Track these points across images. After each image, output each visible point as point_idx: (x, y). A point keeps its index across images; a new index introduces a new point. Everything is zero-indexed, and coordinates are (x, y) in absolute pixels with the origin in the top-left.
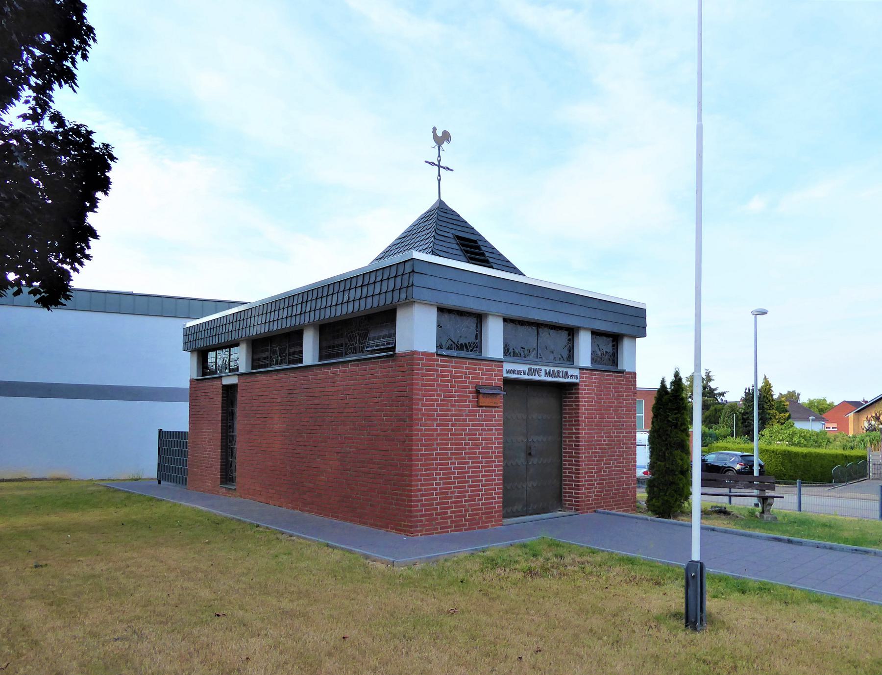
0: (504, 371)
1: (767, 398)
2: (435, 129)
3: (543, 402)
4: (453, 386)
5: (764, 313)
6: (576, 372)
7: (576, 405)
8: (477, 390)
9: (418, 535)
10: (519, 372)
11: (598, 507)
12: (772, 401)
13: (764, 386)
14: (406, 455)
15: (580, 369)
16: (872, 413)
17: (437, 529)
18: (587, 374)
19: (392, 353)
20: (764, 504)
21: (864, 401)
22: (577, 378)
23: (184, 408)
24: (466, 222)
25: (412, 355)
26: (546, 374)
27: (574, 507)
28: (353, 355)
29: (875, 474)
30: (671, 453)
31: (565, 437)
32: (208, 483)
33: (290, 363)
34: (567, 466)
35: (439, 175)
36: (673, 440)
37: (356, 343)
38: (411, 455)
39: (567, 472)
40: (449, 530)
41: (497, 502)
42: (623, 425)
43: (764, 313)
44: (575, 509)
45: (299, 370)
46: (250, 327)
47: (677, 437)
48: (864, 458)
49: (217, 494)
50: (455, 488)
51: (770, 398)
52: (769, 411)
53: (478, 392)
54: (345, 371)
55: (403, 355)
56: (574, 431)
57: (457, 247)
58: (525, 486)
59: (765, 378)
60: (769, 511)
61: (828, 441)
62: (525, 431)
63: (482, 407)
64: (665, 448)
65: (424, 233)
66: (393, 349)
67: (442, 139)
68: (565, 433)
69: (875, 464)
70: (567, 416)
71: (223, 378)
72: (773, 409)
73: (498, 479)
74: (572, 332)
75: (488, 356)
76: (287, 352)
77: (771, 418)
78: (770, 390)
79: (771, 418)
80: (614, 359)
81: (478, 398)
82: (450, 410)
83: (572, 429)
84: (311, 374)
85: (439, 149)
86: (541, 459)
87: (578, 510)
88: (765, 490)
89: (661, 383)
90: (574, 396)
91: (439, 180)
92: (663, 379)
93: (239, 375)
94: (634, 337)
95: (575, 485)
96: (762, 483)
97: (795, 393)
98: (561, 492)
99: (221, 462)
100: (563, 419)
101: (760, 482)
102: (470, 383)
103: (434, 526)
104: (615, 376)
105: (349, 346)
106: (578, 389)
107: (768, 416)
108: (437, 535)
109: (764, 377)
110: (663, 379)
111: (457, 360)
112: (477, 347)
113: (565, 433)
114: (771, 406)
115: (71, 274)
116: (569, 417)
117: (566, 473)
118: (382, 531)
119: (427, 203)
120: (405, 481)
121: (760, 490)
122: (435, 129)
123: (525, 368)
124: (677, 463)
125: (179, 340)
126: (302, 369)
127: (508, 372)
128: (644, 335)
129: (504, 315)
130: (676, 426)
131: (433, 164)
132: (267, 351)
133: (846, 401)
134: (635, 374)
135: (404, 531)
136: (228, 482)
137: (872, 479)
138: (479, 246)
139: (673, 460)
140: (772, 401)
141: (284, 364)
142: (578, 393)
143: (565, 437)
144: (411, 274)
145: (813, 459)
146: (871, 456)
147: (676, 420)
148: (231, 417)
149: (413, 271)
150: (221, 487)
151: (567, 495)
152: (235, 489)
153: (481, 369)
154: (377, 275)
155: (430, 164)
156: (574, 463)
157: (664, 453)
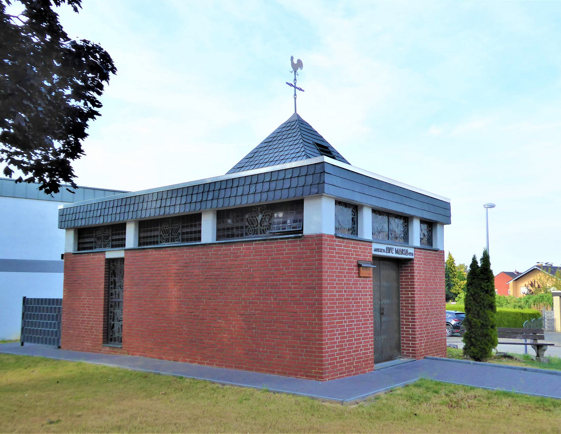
0: (373, 250)
1: (451, 269)
2: (292, 58)
3: (389, 273)
4: (345, 261)
5: (492, 206)
6: (411, 250)
7: (411, 276)
8: (358, 264)
9: (326, 380)
10: (381, 250)
11: (426, 354)
12: (455, 271)
13: (448, 260)
14: (316, 316)
15: (414, 248)
16: (527, 282)
17: (337, 375)
18: (418, 251)
19: (301, 235)
20: (539, 351)
21: (516, 272)
22: (413, 255)
23: (60, 277)
24: (317, 132)
25: (319, 238)
26: (397, 252)
27: (411, 355)
28: (255, 235)
29: (549, 327)
30: (484, 311)
31: (402, 300)
32: (87, 343)
33: (183, 240)
34: (404, 323)
35: (295, 95)
36: (486, 302)
37: (257, 226)
38: (321, 316)
39: (405, 328)
40: (344, 375)
41: (370, 354)
42: (438, 291)
43: (492, 206)
44: (412, 356)
45: (197, 247)
46: (109, 208)
47: (489, 300)
48: (536, 316)
49: (98, 352)
50: (336, 343)
51: (454, 269)
52: (453, 279)
53: (359, 266)
54: (250, 248)
55: (310, 237)
56: (410, 295)
57: (318, 152)
58: (380, 339)
59: (450, 254)
60: (543, 355)
61: (507, 302)
62: (379, 296)
63: (361, 277)
64: (480, 308)
65: (290, 140)
66: (301, 231)
67: (297, 66)
68: (402, 297)
69: (549, 320)
70: (404, 284)
71: (106, 253)
72: (456, 277)
73: (371, 334)
74: (407, 219)
75: (364, 238)
76: (180, 231)
77: (454, 285)
78: (453, 262)
79: (454, 285)
80: (430, 241)
81: (359, 270)
82: (343, 280)
83: (408, 294)
84: (211, 251)
85: (295, 74)
86: (389, 318)
87: (415, 357)
88: (537, 340)
89: (473, 259)
90: (409, 268)
91: (295, 98)
92: (474, 256)
93: (125, 250)
94: (443, 224)
95: (412, 338)
96: (534, 334)
97: (464, 266)
98: (399, 344)
99: (104, 325)
100: (400, 287)
101: (533, 333)
102: (354, 258)
103: (336, 372)
104: (434, 254)
105: (249, 228)
106: (413, 263)
107: (452, 283)
108: (338, 379)
109: (448, 253)
110: (474, 256)
111: (346, 241)
112: (355, 231)
113: (402, 297)
114: (454, 275)
115: (71, 165)
116: (405, 285)
117: (403, 328)
118: (292, 378)
119: (285, 116)
120: (315, 336)
121: (534, 340)
122: (292, 58)
123: (384, 247)
124: (490, 320)
125: (55, 219)
126: (201, 246)
127: (375, 250)
128: (449, 223)
129: (373, 207)
130: (487, 292)
131: (291, 85)
132: (157, 230)
133: (503, 272)
134: (444, 251)
135: (315, 377)
136: (109, 342)
137: (547, 331)
138: (330, 151)
139: (486, 318)
140: (455, 271)
141: (176, 242)
142: (413, 267)
143: (402, 300)
144: (322, 174)
145: (502, 316)
146: (545, 313)
147: (487, 287)
148: (113, 286)
149: (324, 172)
150: (103, 346)
151: (405, 345)
152: (122, 348)
153: (360, 248)
154: (286, 174)
155: (289, 85)
156: (410, 320)
157: (478, 312)
